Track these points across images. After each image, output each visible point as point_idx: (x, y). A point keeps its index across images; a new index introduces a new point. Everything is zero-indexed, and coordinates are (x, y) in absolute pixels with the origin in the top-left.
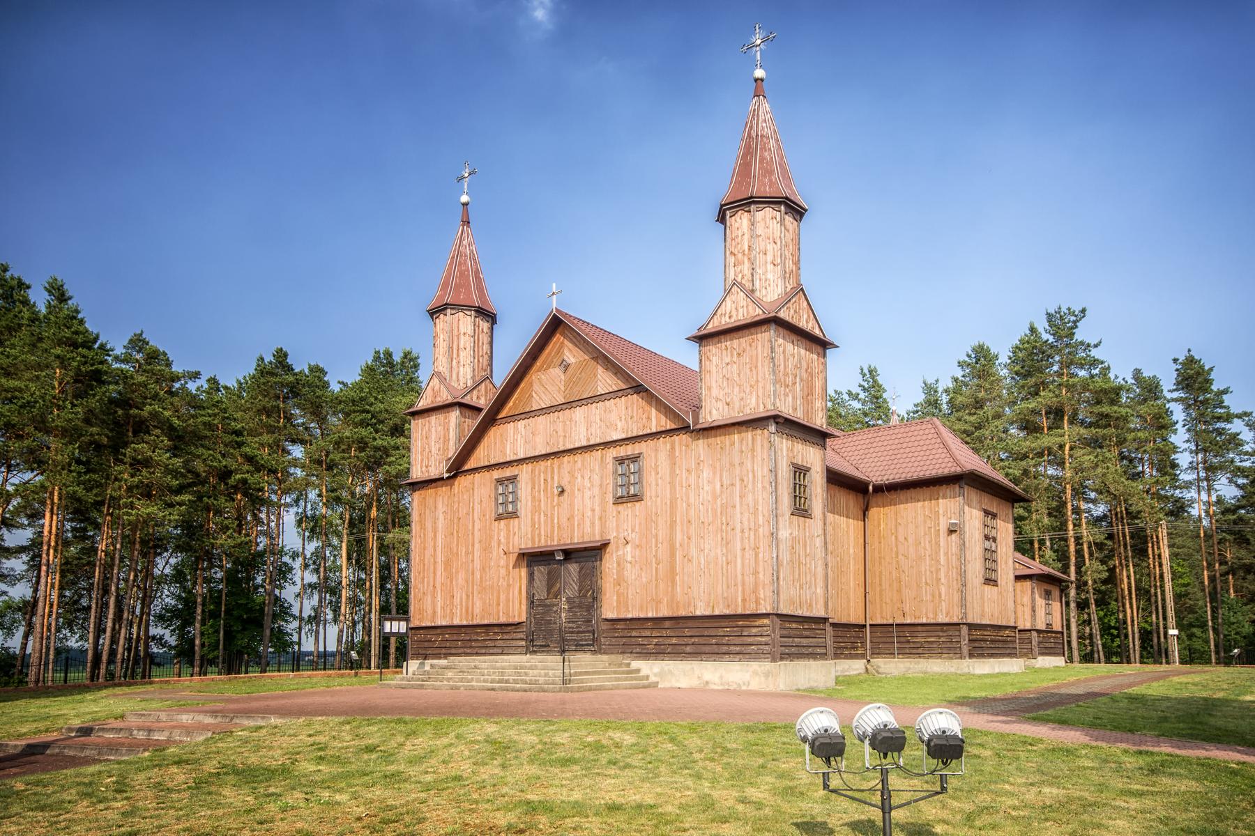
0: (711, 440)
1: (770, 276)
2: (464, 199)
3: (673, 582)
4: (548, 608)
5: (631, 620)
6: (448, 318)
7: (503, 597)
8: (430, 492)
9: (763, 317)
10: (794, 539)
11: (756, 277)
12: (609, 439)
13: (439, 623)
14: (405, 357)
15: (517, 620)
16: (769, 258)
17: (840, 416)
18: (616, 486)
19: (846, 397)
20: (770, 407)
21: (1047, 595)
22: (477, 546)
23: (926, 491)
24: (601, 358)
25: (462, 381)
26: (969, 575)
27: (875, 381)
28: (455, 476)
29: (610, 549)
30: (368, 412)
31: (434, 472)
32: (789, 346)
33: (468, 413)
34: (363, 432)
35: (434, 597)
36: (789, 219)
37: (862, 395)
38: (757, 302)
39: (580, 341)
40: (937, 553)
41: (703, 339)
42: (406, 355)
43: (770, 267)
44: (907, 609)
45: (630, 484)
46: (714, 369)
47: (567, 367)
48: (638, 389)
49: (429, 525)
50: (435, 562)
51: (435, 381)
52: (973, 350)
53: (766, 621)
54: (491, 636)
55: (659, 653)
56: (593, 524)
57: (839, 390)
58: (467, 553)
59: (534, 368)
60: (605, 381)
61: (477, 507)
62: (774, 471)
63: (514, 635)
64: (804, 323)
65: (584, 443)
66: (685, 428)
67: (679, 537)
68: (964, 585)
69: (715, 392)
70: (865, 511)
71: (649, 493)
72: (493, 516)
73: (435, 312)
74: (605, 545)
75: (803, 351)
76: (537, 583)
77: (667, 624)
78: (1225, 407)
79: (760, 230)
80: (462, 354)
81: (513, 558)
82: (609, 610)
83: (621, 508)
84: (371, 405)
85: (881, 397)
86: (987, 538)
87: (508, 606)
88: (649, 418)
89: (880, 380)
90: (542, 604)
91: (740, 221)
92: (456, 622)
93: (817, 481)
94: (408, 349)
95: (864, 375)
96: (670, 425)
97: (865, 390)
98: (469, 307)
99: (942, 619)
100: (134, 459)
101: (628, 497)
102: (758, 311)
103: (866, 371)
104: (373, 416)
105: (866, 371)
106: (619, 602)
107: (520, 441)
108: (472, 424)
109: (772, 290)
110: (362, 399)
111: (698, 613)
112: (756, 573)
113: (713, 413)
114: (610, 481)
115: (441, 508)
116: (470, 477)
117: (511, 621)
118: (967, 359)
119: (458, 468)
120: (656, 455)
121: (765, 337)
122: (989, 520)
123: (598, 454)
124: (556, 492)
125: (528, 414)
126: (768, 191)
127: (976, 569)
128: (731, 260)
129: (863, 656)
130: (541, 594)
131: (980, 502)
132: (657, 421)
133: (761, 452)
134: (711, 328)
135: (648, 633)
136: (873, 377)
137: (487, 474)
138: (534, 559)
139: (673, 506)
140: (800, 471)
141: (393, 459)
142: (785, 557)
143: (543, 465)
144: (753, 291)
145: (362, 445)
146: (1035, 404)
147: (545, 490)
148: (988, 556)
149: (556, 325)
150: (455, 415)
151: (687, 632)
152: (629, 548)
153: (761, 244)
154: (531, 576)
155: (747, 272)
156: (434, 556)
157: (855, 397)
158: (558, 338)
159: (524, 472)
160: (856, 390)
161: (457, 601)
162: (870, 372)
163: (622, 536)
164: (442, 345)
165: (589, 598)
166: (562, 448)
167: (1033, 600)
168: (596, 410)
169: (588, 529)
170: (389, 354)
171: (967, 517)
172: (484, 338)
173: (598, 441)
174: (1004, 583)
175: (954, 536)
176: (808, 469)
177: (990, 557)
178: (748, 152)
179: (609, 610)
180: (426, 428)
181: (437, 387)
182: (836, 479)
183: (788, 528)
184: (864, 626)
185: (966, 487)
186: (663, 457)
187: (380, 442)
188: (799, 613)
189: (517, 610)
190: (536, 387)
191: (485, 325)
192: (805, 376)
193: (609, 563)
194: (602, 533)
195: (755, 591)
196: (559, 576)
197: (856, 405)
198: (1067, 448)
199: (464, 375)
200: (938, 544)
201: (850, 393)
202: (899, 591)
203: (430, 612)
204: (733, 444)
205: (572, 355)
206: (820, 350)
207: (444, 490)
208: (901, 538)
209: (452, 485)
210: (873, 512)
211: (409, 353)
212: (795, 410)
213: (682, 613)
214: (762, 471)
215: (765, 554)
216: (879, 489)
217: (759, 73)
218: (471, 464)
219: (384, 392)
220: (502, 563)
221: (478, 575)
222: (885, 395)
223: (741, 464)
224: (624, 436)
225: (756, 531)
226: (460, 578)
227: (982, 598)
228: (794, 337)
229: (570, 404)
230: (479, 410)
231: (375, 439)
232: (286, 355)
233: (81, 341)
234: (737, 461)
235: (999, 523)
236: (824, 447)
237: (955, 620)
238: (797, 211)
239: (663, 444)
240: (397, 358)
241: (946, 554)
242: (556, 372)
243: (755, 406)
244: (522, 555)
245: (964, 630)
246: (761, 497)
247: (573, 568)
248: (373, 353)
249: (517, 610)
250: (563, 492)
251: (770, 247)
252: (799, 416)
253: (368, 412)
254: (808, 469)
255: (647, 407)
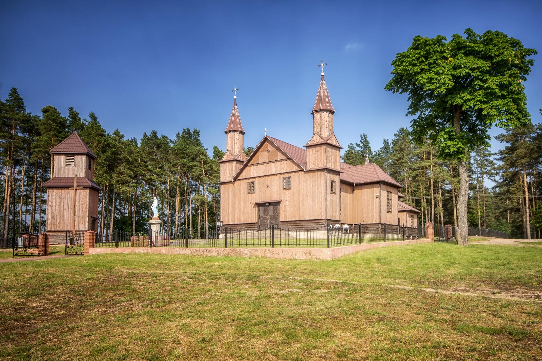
0: (310, 174)
1: (325, 130)
2: (235, 97)
3: (299, 211)
4: (264, 219)
5: (288, 221)
6: (232, 134)
7: (250, 216)
8: (226, 185)
9: (323, 142)
10: (331, 200)
11: (322, 131)
12: (281, 172)
13: (230, 223)
14: (195, 132)
15: (254, 222)
16: (325, 126)
17: (352, 153)
18: (283, 185)
19: (355, 146)
20: (325, 166)
21: (412, 216)
22: (242, 201)
23: (370, 186)
24: (278, 149)
25: (236, 153)
26: (382, 210)
27: (366, 140)
28: (235, 181)
29: (282, 202)
30: (185, 153)
31: (228, 179)
32: (330, 149)
33: (238, 162)
34: (185, 161)
35: (229, 216)
36: (330, 115)
37: (361, 145)
38: (322, 138)
39: (273, 145)
40: (373, 203)
41: (307, 147)
42: (195, 131)
43: (325, 128)
44: (364, 220)
45: (287, 185)
46: (310, 155)
47: (269, 151)
48: (290, 159)
49: (226, 195)
50: (229, 206)
51: (228, 153)
52: (400, 130)
53: (324, 221)
54: (247, 227)
55: (296, 230)
56: (277, 195)
57: (352, 143)
58: (239, 203)
59: (259, 151)
60: (280, 156)
61: (242, 190)
62: (326, 182)
63: (254, 226)
64: (334, 143)
65: (274, 173)
66: (303, 170)
67: (301, 199)
68: (380, 213)
69: (311, 161)
70: (353, 191)
71: (293, 187)
72: (247, 193)
73: (227, 132)
74: (281, 201)
75: (334, 150)
76: (261, 211)
77: (298, 222)
78: (488, 151)
79: (323, 118)
80: (236, 145)
81: (253, 205)
82: (282, 218)
83: (285, 191)
84: (185, 150)
85: (368, 146)
86: (388, 199)
87: (252, 218)
88: (293, 167)
89: (368, 139)
90: (262, 217)
91: (318, 115)
92: (236, 223)
93: (338, 185)
94: (196, 129)
95: (362, 137)
96: (299, 169)
97: (362, 143)
98: (238, 131)
99: (374, 222)
100: (119, 172)
101: (287, 188)
102: (322, 141)
103: (362, 136)
104: (187, 155)
105: (362, 136)
106: (284, 216)
107: (255, 172)
108: (240, 166)
109: (326, 134)
110: (183, 149)
111: (306, 219)
112: (321, 209)
113: (310, 167)
114: (282, 184)
115: (230, 190)
116: (239, 182)
117: (253, 222)
118: (398, 133)
119: (236, 179)
120: (295, 177)
121: (324, 148)
122: (389, 194)
123: (278, 176)
124: (266, 186)
125: (258, 164)
126: (325, 108)
127: (384, 208)
128: (315, 126)
129: (351, 233)
130: (262, 214)
131: (386, 189)
132: (295, 168)
133: (323, 178)
134: (310, 144)
135: (292, 225)
136: (365, 138)
137: (245, 181)
138: (259, 205)
139: (299, 190)
140: (333, 182)
141: (194, 170)
142: (329, 204)
143: (262, 178)
144: (321, 135)
145: (184, 165)
146: (420, 151)
147: (263, 186)
148: (389, 204)
149: (266, 140)
150: (234, 163)
151: (303, 224)
152: (287, 202)
153: (323, 122)
154: (259, 210)
155: (319, 129)
156: (229, 204)
157: (358, 145)
158: (266, 143)
159: (256, 181)
160: (359, 143)
161: (236, 217)
162: (364, 136)
163: (285, 199)
164: (229, 142)
165: (276, 216)
166: (268, 174)
167: (406, 218)
168: (278, 164)
169: (275, 197)
170: (188, 130)
171: (381, 193)
172: (241, 140)
173: (278, 173)
174: (394, 212)
175: (378, 199)
176: (335, 182)
177: (389, 205)
178: (320, 96)
179: (282, 218)
180: (225, 167)
181: (229, 155)
182: (342, 182)
183: (330, 197)
184: (352, 225)
185: (381, 185)
186: (297, 178)
187: (190, 164)
188: (332, 219)
189: (255, 219)
190: (260, 156)
191: (242, 136)
192: (334, 157)
193: (282, 206)
194: (280, 198)
195: (321, 213)
196: (267, 210)
197: (359, 149)
198: (432, 166)
199: (236, 151)
200: (373, 201)
201: (356, 144)
202: (363, 215)
203: (227, 220)
204: (315, 175)
205: (271, 148)
206: (339, 149)
207: (231, 185)
208: (363, 199)
209: (234, 184)
210: (355, 191)
211: (196, 130)
212: (332, 166)
213: (302, 219)
214: (323, 182)
215: (324, 204)
216: (357, 185)
217: (323, 74)
218: (240, 178)
219: (188, 145)
220: (250, 206)
221: (242, 209)
222: (369, 145)
223: (318, 180)
224: (286, 172)
225: (321, 198)
226: (237, 210)
227: (386, 216)
228: (331, 147)
229: (270, 162)
230: (243, 162)
231: (188, 163)
232: (156, 133)
233: (102, 134)
234: (316, 179)
235: (393, 195)
236: (339, 175)
237: (378, 223)
238: (332, 112)
239: (297, 174)
240: (192, 132)
241: (375, 204)
242: (266, 153)
243: (321, 165)
244: (256, 204)
245: (380, 225)
246: (323, 189)
247: (271, 207)
248: (183, 130)
249: (255, 219)
250: (268, 187)
251: (325, 123)
252: (333, 168)
253: (185, 153)
254: (335, 182)
255: (292, 164)
